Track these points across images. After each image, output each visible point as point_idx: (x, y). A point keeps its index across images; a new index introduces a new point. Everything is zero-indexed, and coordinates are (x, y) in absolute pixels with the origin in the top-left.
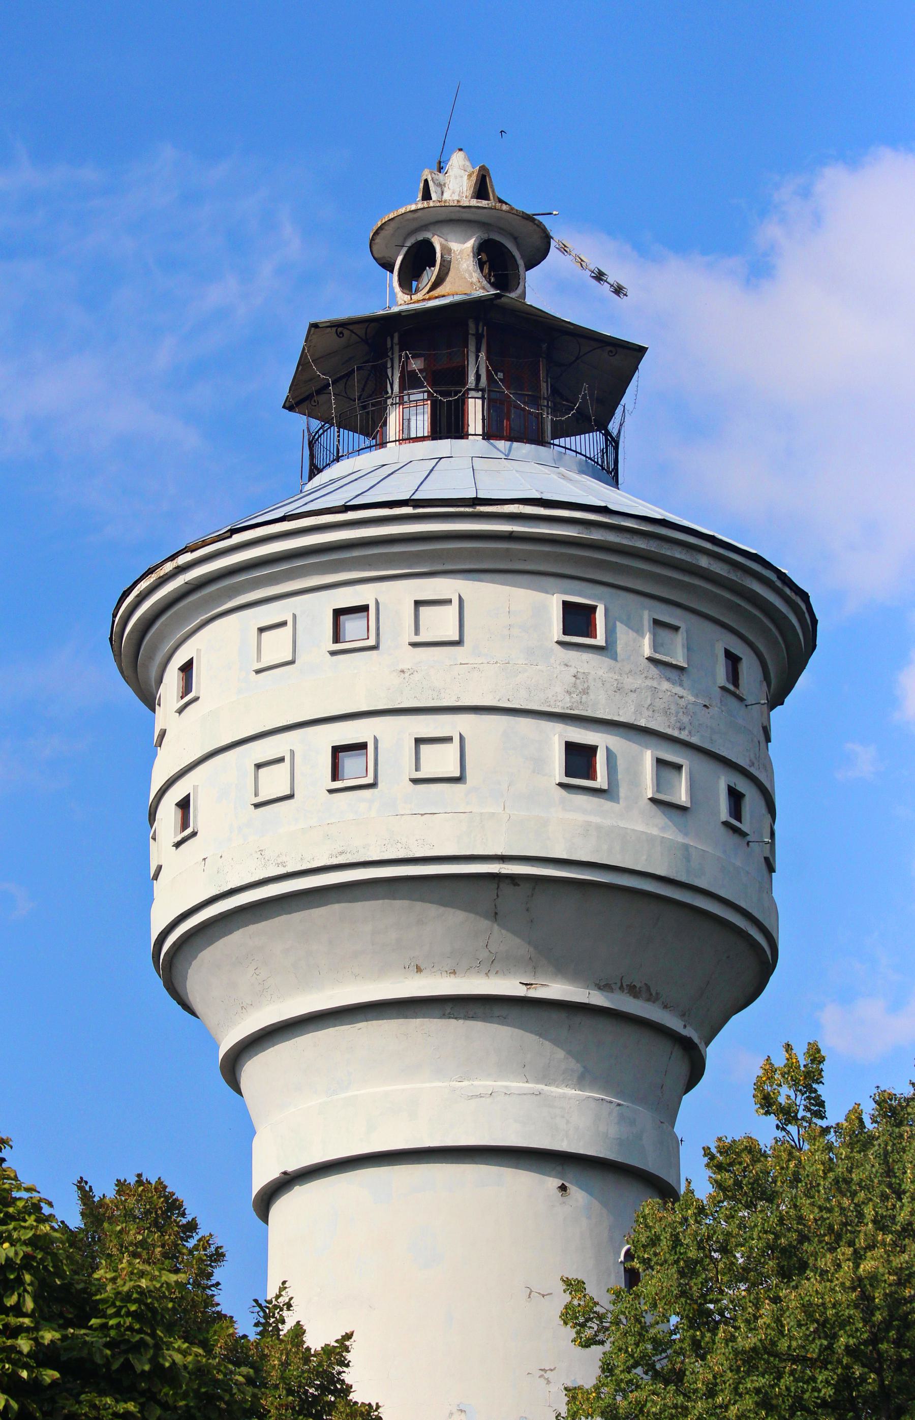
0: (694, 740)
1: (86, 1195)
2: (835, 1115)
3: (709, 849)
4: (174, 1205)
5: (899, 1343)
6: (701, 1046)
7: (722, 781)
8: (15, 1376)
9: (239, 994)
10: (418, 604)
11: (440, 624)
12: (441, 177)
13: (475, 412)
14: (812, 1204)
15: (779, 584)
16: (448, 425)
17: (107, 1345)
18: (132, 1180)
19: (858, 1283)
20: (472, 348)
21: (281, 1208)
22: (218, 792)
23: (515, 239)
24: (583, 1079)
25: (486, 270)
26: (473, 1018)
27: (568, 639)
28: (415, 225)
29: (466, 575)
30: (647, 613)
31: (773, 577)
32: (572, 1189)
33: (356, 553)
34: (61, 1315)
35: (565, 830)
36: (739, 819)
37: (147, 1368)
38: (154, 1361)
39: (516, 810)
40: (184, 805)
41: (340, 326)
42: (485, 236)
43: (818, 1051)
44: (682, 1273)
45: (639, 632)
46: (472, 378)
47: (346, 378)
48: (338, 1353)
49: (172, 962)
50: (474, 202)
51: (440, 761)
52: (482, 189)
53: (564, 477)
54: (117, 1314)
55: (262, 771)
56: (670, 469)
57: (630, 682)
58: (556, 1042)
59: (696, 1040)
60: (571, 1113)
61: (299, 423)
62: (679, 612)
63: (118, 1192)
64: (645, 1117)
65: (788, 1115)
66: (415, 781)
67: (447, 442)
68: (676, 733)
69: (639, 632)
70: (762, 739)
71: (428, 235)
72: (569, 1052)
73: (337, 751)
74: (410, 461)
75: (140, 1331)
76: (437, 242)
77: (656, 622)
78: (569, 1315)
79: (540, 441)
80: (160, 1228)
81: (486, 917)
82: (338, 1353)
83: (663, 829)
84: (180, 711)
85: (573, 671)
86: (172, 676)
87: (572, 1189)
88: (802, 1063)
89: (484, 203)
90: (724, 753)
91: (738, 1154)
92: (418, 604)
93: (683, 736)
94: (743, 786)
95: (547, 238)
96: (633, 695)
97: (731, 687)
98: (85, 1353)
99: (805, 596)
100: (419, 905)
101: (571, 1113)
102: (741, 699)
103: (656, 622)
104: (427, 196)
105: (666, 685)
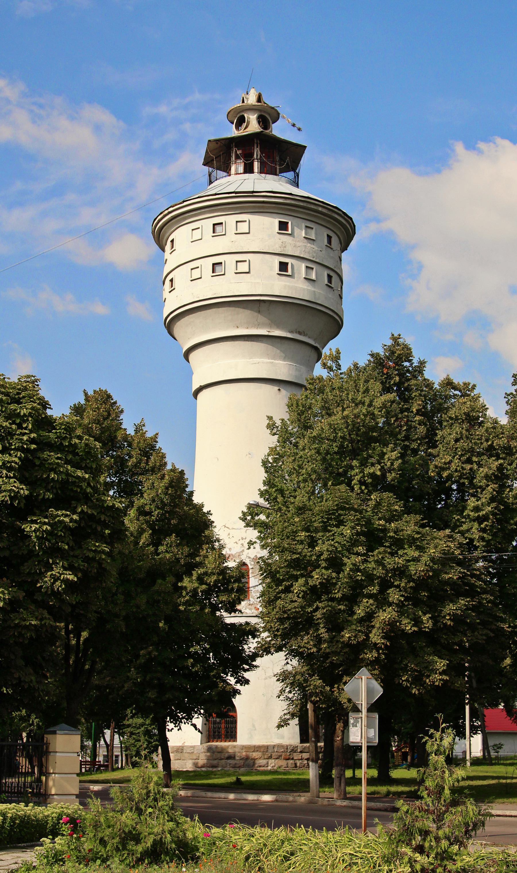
0: (317, 261)
1: (86, 394)
2: (344, 369)
3: (322, 292)
4: (109, 397)
5: (357, 435)
6: (321, 349)
7: (326, 273)
8: (23, 447)
9: (189, 333)
10: (237, 222)
11: (243, 227)
12: (247, 96)
13: (256, 165)
14: (332, 395)
15: (343, 215)
16: (249, 169)
17: (56, 438)
18: (98, 390)
19: (343, 418)
20: (255, 147)
21: (200, 396)
22: (181, 277)
23: (269, 114)
24: (284, 359)
25: (261, 124)
26: (253, 341)
27: (280, 232)
28: (239, 111)
29: (261, 214)
30: (304, 224)
31: (341, 213)
32: (282, 390)
33: (219, 207)
34: (48, 429)
35: (279, 287)
36: (331, 283)
37: (67, 444)
38: (69, 442)
39: (265, 281)
40: (171, 280)
41: (217, 141)
42: (260, 114)
43: (339, 351)
44: (298, 414)
45: (301, 229)
46: (255, 156)
47: (220, 155)
48: (155, 439)
49: (170, 325)
50: (256, 104)
51: (243, 267)
52: (259, 100)
53: (281, 184)
54: (60, 429)
55: (193, 271)
56: (314, 182)
57: (298, 244)
58: (277, 348)
59: (319, 347)
60: (282, 368)
61: (206, 168)
62: (313, 223)
63: (94, 393)
64: (303, 369)
65: (330, 369)
66: (236, 273)
67: (247, 174)
68: (312, 259)
69: (301, 229)
70: (339, 260)
71: (243, 114)
72: (281, 351)
73: (214, 265)
74: (238, 180)
75: (66, 434)
76: (246, 115)
77: (306, 227)
78: (268, 426)
79: (276, 174)
80: (105, 403)
81: (256, 312)
82: (155, 439)
83: (308, 286)
84: (171, 253)
85: (282, 241)
86: (169, 243)
87: (282, 390)
88: (334, 354)
89: (259, 104)
90: (326, 264)
91: (315, 380)
92: (237, 222)
93: (314, 259)
94: (332, 274)
95: (279, 114)
96: (299, 248)
97: (329, 245)
98: (49, 440)
99: (351, 219)
100: (237, 309)
101: (282, 368)
102: (332, 249)
103: (306, 227)
104: (243, 102)
105: (309, 245)
